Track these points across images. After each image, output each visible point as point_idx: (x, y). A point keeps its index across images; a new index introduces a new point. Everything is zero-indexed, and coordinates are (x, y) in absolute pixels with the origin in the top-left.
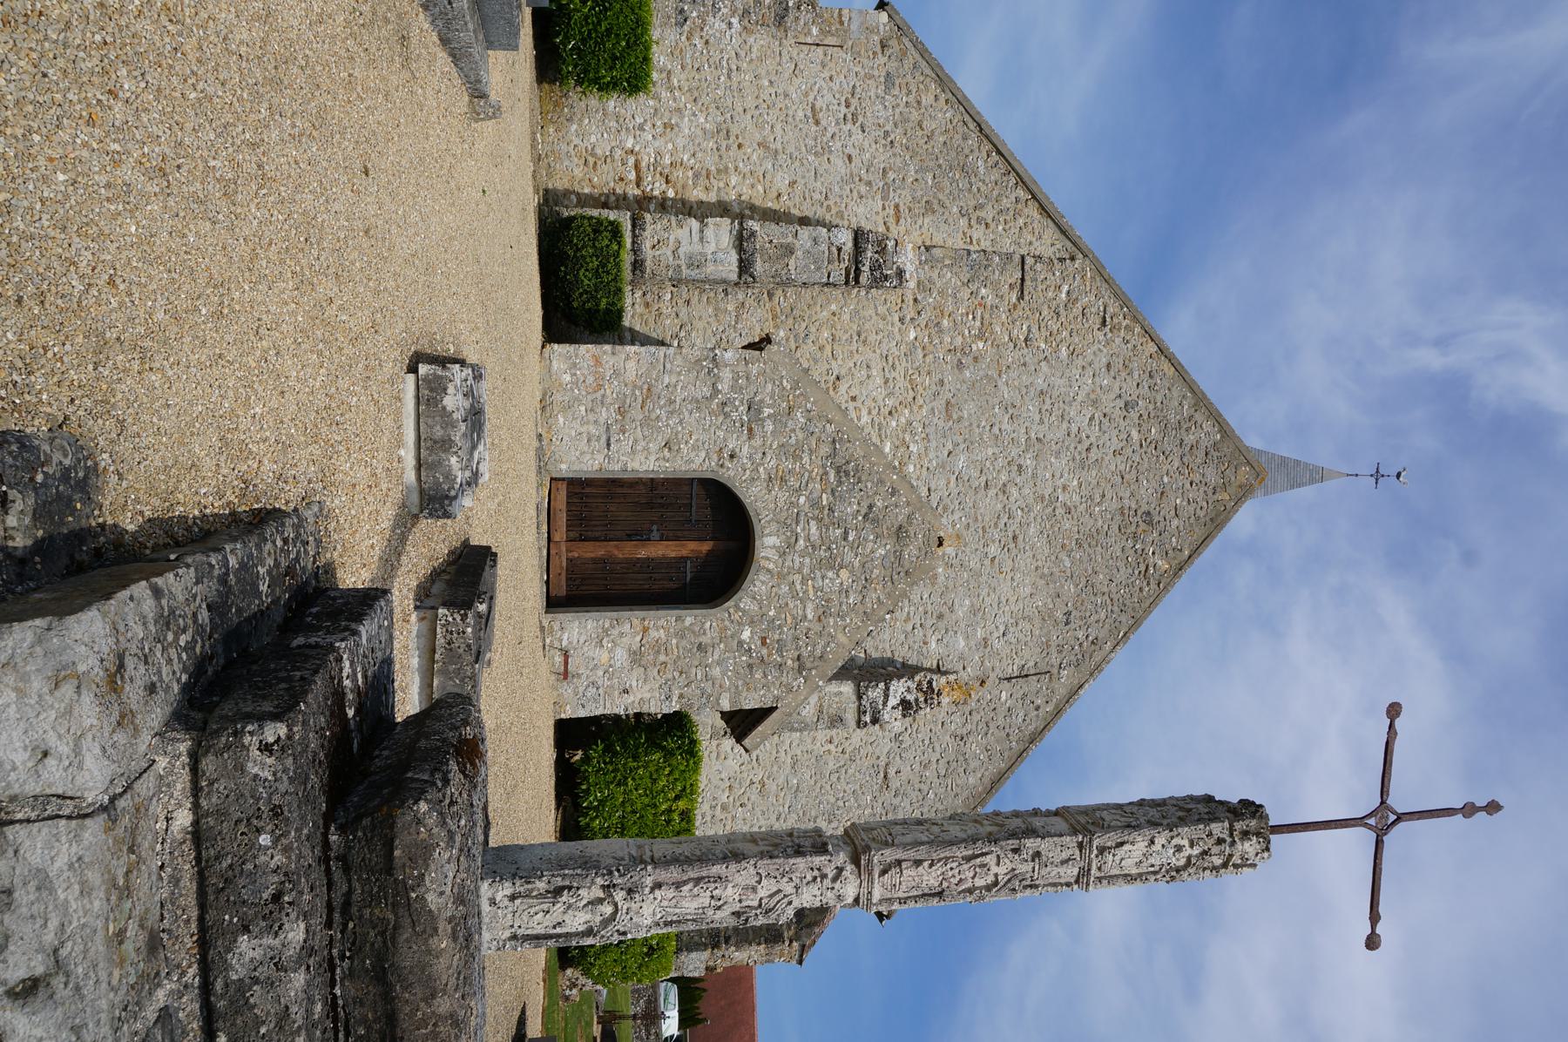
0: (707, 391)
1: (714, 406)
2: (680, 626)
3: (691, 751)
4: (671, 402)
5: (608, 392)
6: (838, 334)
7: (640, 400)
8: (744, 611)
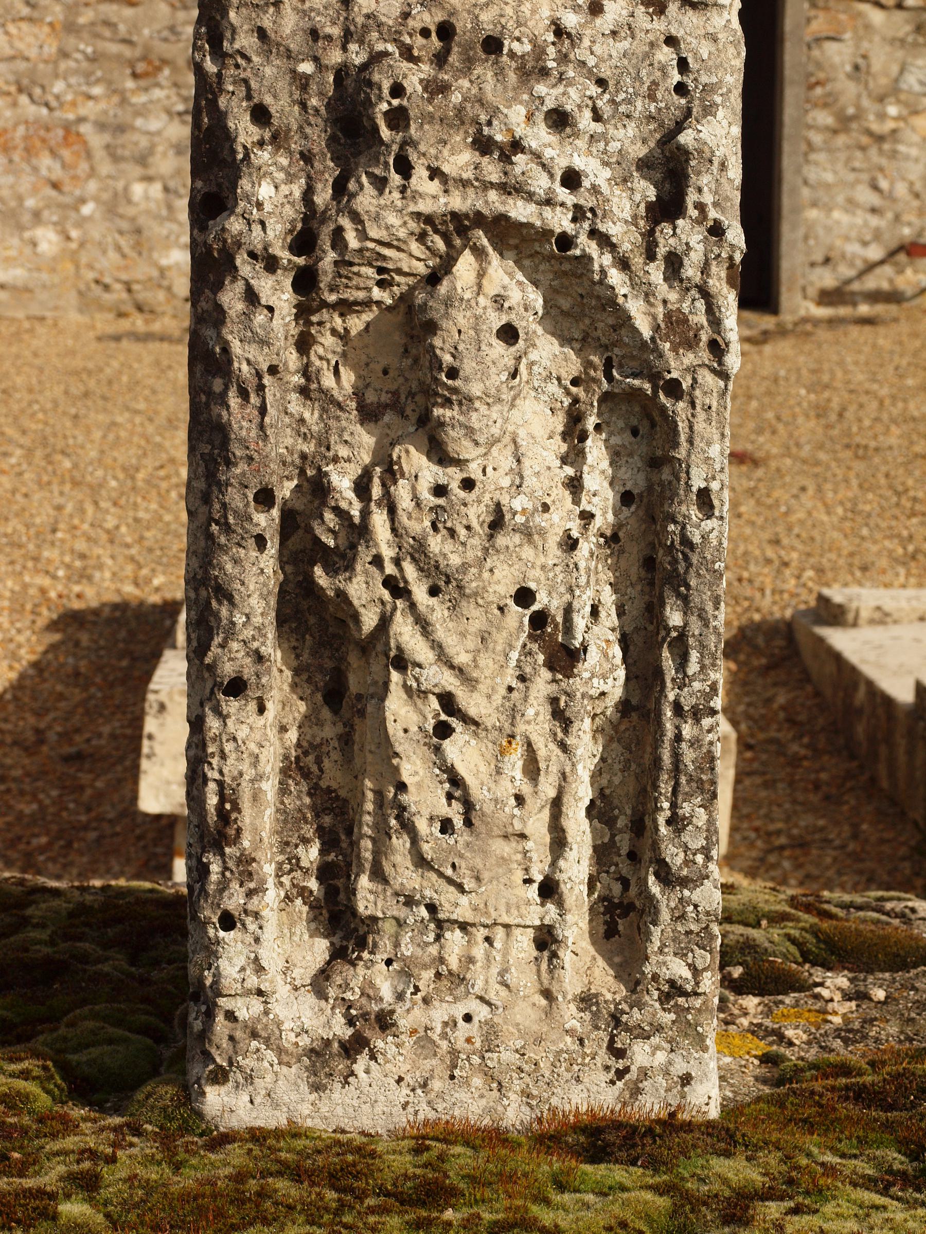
5: (89, 109)
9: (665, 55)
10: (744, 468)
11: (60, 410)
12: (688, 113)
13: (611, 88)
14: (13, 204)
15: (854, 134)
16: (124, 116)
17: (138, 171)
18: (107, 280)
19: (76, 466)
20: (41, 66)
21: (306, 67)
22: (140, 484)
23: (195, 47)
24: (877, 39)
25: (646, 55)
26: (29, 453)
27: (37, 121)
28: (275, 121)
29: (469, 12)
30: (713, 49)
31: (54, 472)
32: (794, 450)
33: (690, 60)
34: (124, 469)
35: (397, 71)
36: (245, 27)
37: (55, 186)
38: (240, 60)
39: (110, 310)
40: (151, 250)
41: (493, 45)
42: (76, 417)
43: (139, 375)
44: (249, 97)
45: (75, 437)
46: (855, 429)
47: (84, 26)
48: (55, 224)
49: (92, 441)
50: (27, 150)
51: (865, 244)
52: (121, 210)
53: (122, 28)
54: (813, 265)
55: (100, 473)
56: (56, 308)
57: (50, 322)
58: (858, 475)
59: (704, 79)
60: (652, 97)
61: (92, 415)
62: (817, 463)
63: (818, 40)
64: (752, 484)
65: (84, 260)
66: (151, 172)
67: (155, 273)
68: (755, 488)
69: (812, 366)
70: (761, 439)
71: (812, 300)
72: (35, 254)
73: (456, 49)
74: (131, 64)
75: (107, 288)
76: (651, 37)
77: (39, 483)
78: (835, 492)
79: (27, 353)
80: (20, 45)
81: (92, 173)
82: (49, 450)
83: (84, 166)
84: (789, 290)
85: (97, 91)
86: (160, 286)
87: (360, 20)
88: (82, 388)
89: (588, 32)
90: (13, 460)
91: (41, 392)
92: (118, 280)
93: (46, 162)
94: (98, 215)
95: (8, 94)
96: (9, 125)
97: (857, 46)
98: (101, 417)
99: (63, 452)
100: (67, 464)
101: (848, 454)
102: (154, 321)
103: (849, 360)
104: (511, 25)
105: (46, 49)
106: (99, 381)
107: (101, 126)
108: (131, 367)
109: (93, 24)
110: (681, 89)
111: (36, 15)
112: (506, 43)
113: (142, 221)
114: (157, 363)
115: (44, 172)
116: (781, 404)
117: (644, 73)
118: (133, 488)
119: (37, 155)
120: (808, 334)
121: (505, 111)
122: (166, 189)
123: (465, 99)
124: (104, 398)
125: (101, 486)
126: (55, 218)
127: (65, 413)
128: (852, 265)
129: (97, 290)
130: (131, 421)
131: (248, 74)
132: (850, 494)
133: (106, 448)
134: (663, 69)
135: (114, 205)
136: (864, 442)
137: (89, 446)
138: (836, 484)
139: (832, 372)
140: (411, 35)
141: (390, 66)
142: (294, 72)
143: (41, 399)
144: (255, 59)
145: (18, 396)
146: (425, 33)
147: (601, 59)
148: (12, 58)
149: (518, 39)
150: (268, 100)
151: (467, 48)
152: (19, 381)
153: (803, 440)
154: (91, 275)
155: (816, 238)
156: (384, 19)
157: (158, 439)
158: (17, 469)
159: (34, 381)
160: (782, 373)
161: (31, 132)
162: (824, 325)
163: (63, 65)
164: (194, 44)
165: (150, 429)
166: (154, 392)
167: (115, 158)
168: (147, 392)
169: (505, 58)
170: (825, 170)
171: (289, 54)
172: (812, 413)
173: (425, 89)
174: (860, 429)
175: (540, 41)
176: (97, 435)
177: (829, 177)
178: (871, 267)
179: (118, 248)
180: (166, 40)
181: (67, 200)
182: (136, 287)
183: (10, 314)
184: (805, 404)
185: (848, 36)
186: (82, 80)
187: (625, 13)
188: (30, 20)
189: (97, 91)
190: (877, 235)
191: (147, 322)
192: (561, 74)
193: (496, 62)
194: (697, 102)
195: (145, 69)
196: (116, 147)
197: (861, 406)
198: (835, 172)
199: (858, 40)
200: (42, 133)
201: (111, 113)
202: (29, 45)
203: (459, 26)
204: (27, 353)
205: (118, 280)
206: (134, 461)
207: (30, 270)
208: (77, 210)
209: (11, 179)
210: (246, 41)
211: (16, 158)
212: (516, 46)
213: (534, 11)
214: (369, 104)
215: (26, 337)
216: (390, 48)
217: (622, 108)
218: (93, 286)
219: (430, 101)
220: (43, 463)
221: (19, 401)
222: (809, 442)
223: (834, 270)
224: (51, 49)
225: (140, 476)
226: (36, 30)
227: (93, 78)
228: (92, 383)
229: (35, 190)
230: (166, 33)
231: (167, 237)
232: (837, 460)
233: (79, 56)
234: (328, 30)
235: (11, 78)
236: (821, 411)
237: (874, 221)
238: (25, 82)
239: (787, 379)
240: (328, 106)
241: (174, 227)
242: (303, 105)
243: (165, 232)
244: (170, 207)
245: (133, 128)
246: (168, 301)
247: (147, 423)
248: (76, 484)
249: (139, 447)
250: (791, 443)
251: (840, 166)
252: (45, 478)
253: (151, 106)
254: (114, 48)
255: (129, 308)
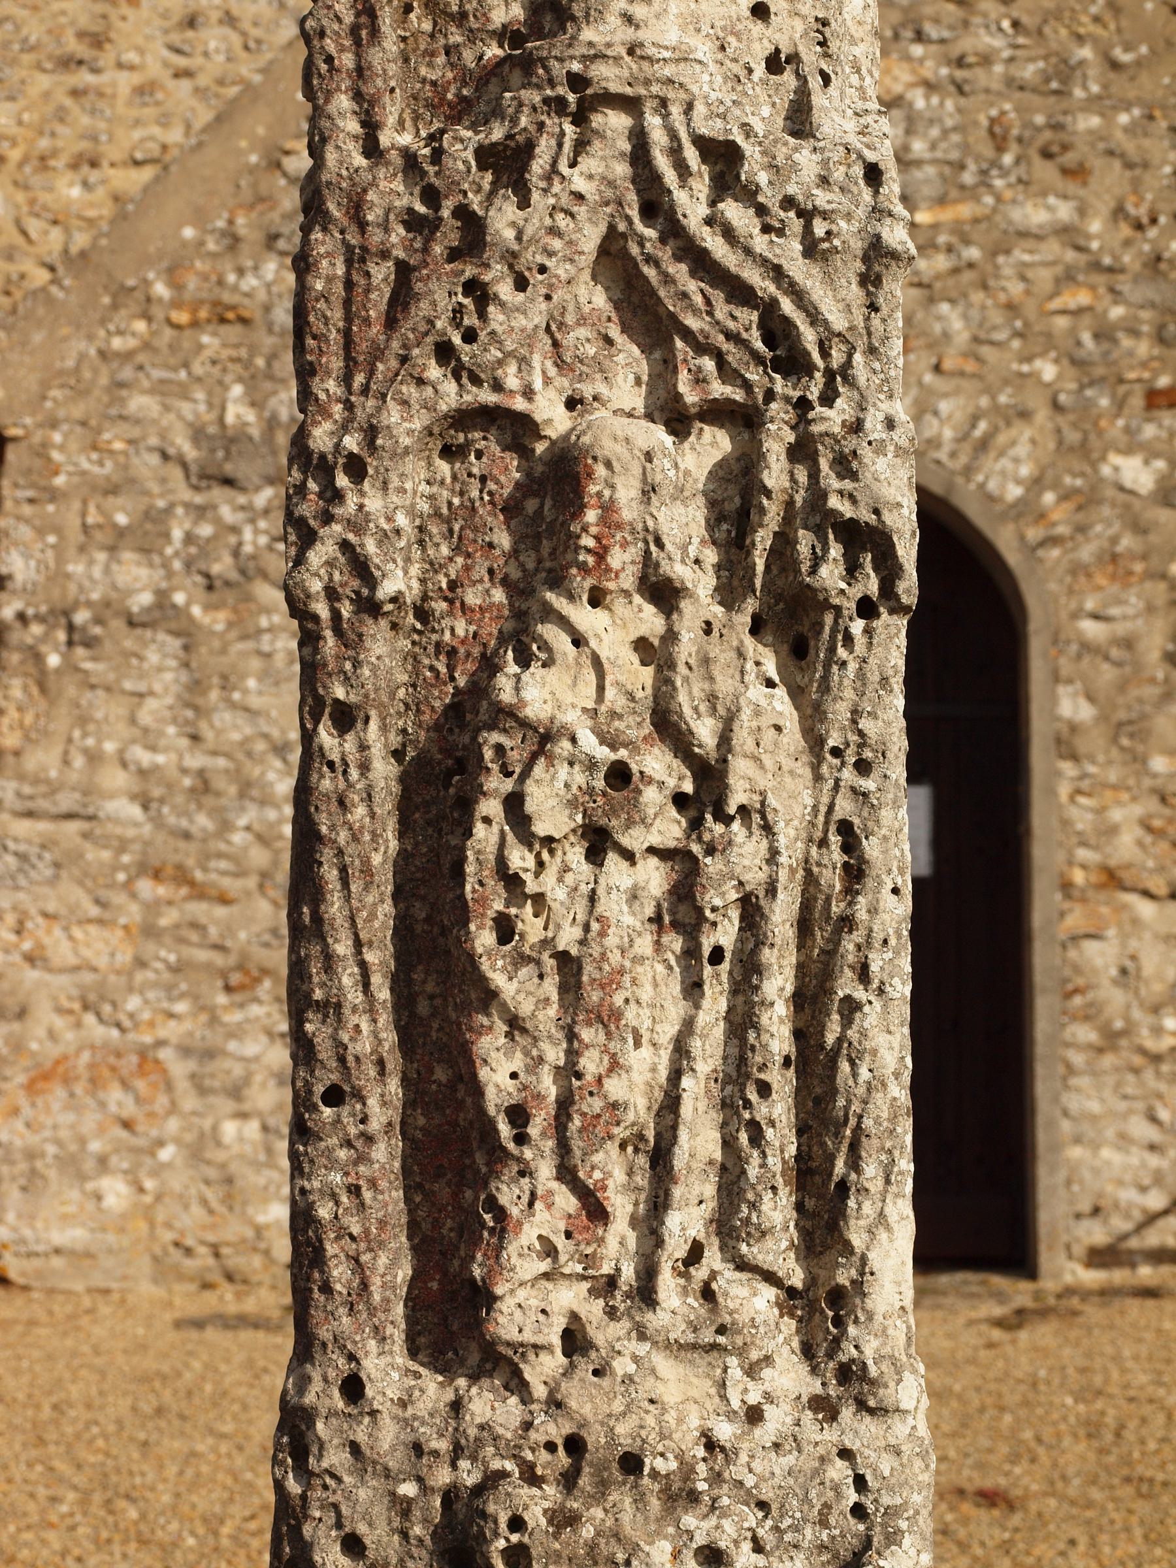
0: (160, 653)
1: (218, 621)
2: (1094, 742)
3: (202, 468)
4: (204, 786)
5: (171, 1030)
6: (68, 140)
7: (199, 910)
8: (1036, 484)
9: (839, 1470)
10: (996, 1513)
11: (125, 1435)
12: (867, 1543)
13: (775, 1512)
14: (73, 1147)
15: (1124, 1054)
16: (214, 1038)
17: (229, 1106)
18: (189, 1242)
19: (143, 1516)
20: (112, 978)
21: (408, 1489)
22: (225, 1542)
23: (275, 1461)
24: (1147, 936)
25: (816, 1472)
26: (84, 1501)
27: (106, 1045)
28: (370, 1554)
29: (602, 1424)
30: (896, 1464)
31: (116, 1525)
32: (1060, 1485)
33: (868, 1478)
34: (205, 1520)
35: (516, 1501)
36: (336, 1441)
37: (127, 1125)
38: (328, 1480)
39: (191, 1279)
40: (245, 1203)
41: (631, 1464)
42: (145, 1444)
43: (228, 1380)
44: (339, 1525)
45: (143, 1474)
46: (1136, 1455)
47: (165, 929)
48: (125, 1172)
49: (165, 1480)
50: (93, 1081)
51: (1143, 1189)
52: (208, 1155)
53: (213, 931)
54: (1078, 1216)
55: (174, 1526)
56: (125, 1278)
57: (116, 1297)
58: (1142, 1522)
59: (886, 1500)
60: (823, 1523)
61: (166, 1441)
62: (1090, 1505)
63: (1075, 939)
64: (1007, 1535)
65: (160, 1216)
66: (246, 1107)
67: (250, 1233)
68: (1011, 1541)
69: (1081, 1362)
70: (1017, 1470)
71: (1079, 1260)
72: (100, 1209)
73: (587, 1469)
74: (224, 974)
75: (188, 1252)
76: (821, 1450)
77: (96, 1541)
78: (1114, 1547)
79: (85, 1349)
80: (87, 953)
81: (173, 1108)
82: (109, 1494)
83: (162, 1101)
84: (1050, 1248)
85: (181, 1007)
86: (255, 1249)
87: (472, 1432)
88: (155, 1404)
89: (745, 1445)
90: (64, 1508)
91: (102, 1408)
92: (203, 1243)
93: (115, 1096)
94: (179, 1162)
95: (70, 1012)
96: (71, 1050)
97: (1123, 945)
98: (177, 1444)
99: (127, 1497)
100: (133, 1514)
101: (1129, 1490)
102: (247, 1294)
103: (1127, 1353)
104: (653, 1438)
105: (119, 958)
106: (175, 1392)
107: (185, 1051)
108: (216, 1370)
109: (177, 926)
110: (858, 1511)
111: (107, 916)
112: (647, 1461)
113: (234, 1167)
114: (249, 1364)
115: (113, 1108)
116: (1041, 1419)
117: (813, 1494)
118: (216, 1549)
119: (104, 1087)
120: (1075, 1313)
121: (647, 1548)
122: (265, 1128)
123: (598, 1534)
124: (182, 1417)
125: (175, 1545)
126: (125, 1165)
127: (132, 1439)
128: (1127, 1216)
129: (176, 1255)
130: (214, 1450)
131: (338, 1498)
132: (1133, 1550)
133: (182, 1489)
134: (836, 1488)
135: (199, 1148)
136: (1149, 1473)
137: (161, 1487)
138: (1115, 1535)
139: (1105, 1370)
140: (533, 1450)
141: (508, 1494)
142: (393, 1494)
143: (101, 1418)
144: (348, 1479)
145: (72, 1413)
146: (551, 1447)
147: (762, 1478)
148: (76, 969)
149: (662, 1455)
150: (362, 1529)
151: (601, 1468)
152: (75, 1391)
153: (1071, 1471)
154: (168, 1236)
155: (1081, 1182)
156: (501, 1431)
157: (249, 1476)
158: (69, 1521)
159: (94, 1391)
160: (1042, 1373)
161: (98, 1058)
162: (1096, 1299)
163: (140, 977)
164: (275, 1457)
165: (239, 1461)
166: (245, 1407)
167: (202, 1091)
168: (236, 1407)
169: (646, 1481)
170: (1089, 1097)
171: (387, 1473)
172: (1082, 1433)
173: (550, 1522)
174: (1143, 1454)
175: (688, 1458)
176: (172, 1470)
177: (1095, 1107)
178: (1151, 1219)
179: (204, 1202)
180: (267, 945)
181: (140, 1142)
182: (225, 1251)
183: (65, 1285)
184: (1072, 1420)
185: (1111, 932)
186: (163, 994)
187: (789, 1420)
188: (100, 922)
189: (181, 1007)
190: (1158, 1179)
191: (239, 1296)
192: (714, 1500)
193: (636, 1486)
194: (878, 1529)
195: (240, 982)
196: (203, 1077)
197: (1144, 1421)
198: (1102, 1100)
199: (1124, 937)
200: (112, 1060)
201: (198, 1034)
202: (98, 953)
203: (590, 1441)
204: (85, 1349)
205: (203, 1243)
206: (217, 1509)
207: (92, 1230)
208: (153, 1154)
209: (70, 1117)
210: (336, 1458)
211: (79, 1090)
212: (659, 1464)
213: (680, 1421)
214: (482, 1539)
215: (85, 1321)
216: (509, 1466)
217: (788, 1537)
218: (171, 1249)
219: (556, 1536)
220: (102, 1513)
221: (74, 1421)
222: (1078, 1474)
223: (1105, 1222)
224: (125, 957)
225: (226, 1530)
226: (106, 934)
227: (175, 993)
228: (167, 1396)
229: (101, 1130)
230: (267, 937)
231: (266, 1188)
232: (1114, 1499)
233: (159, 965)
234: (434, 1444)
235: (75, 992)
236: (1092, 1428)
237: (1154, 1161)
238: (92, 997)
239: (1048, 1383)
240: (434, 1535)
241: (275, 1175)
242: (404, 1535)
243: (262, 1181)
244: (269, 1151)
245: (224, 1053)
246: (266, 1268)
247: (234, 1452)
248: (143, 1542)
249: (225, 1488)
250: (1056, 1475)
251: (1107, 1093)
252: (105, 1534)
253: (247, 1027)
254: (203, 956)
255: (216, 1277)
